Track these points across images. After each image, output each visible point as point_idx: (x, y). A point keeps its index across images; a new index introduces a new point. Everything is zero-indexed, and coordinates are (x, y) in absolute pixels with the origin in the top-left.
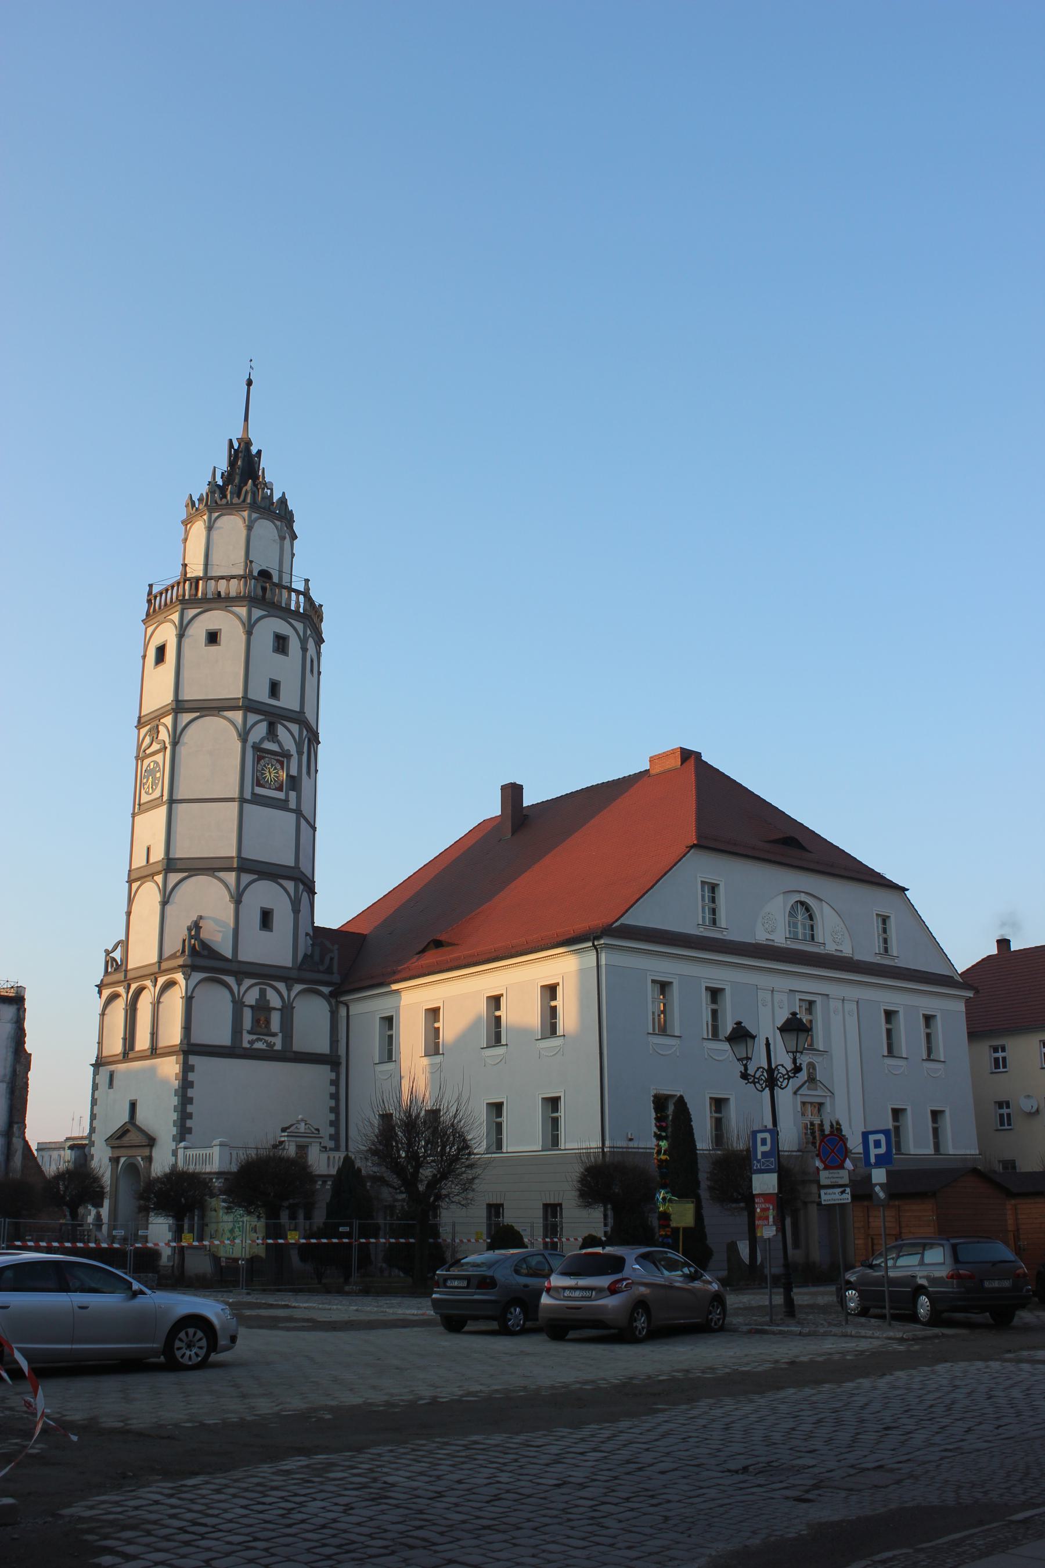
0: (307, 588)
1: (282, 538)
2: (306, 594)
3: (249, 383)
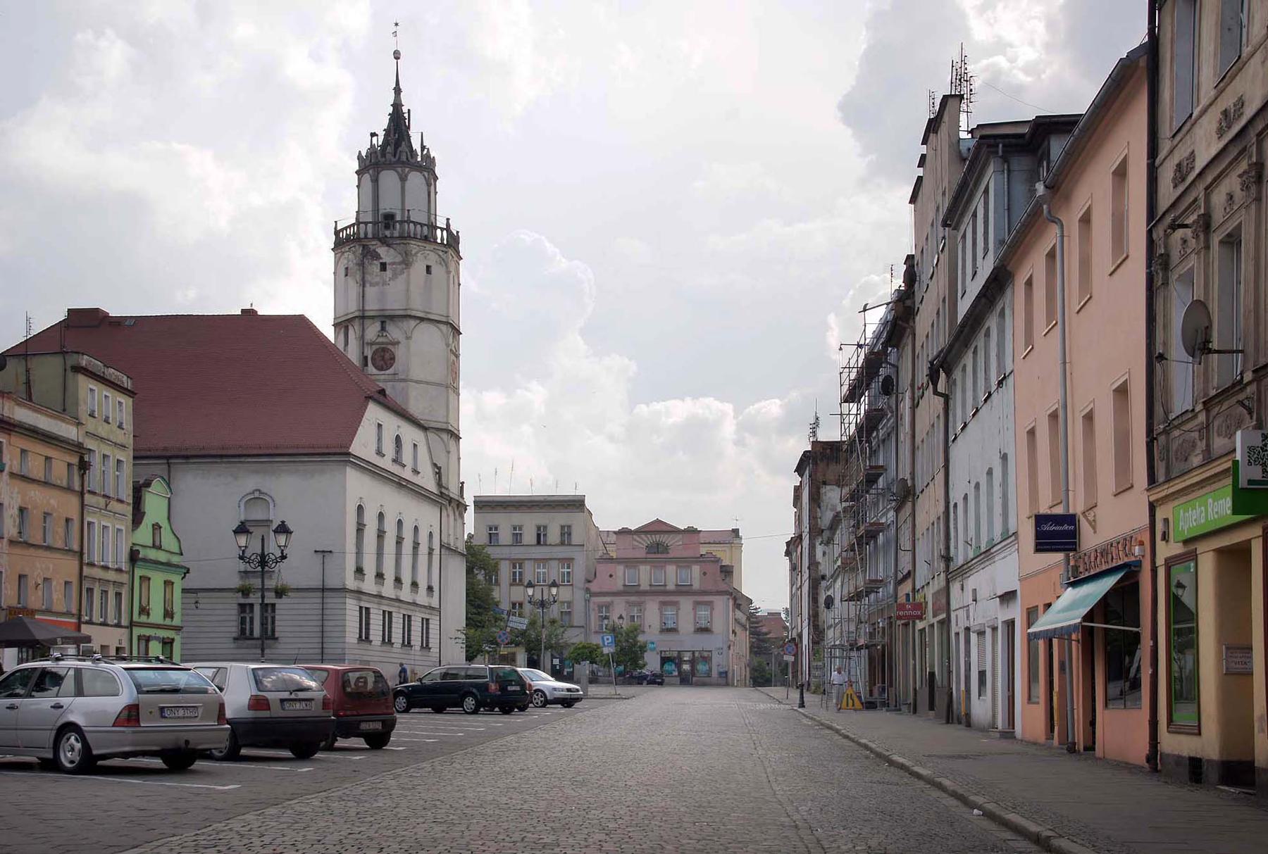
0: (448, 225)
1: (429, 185)
2: (448, 228)
3: (397, 55)
